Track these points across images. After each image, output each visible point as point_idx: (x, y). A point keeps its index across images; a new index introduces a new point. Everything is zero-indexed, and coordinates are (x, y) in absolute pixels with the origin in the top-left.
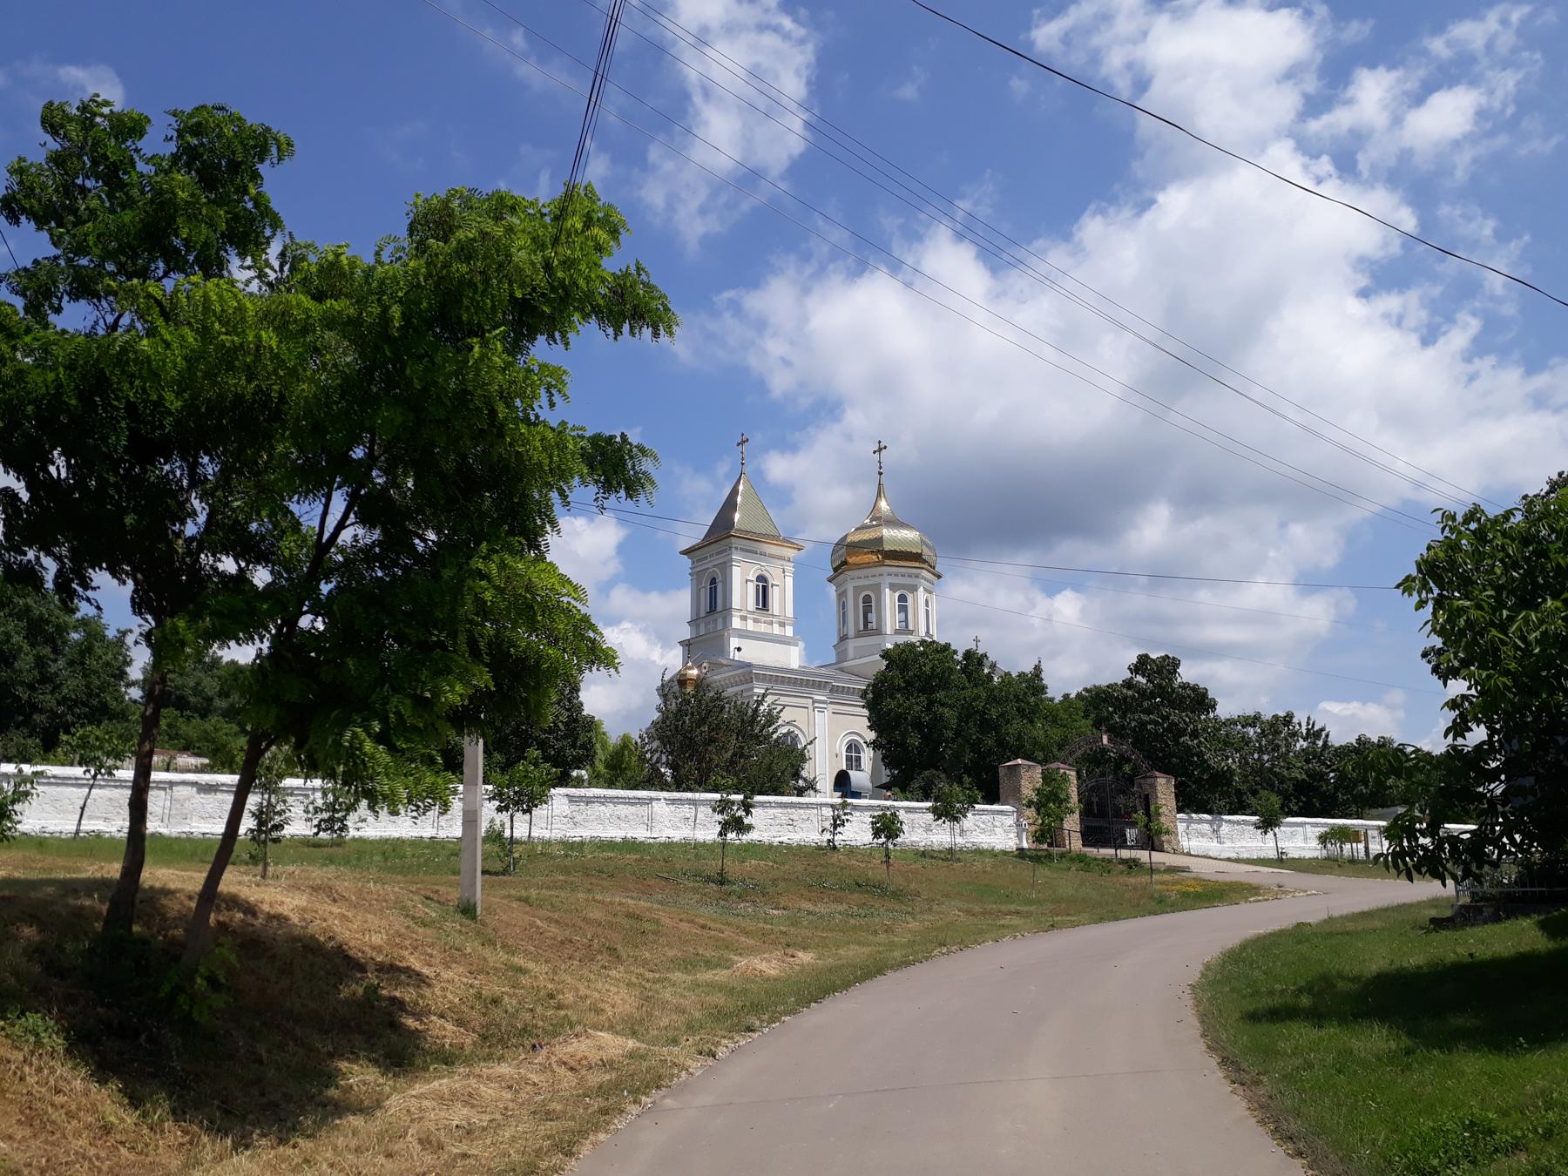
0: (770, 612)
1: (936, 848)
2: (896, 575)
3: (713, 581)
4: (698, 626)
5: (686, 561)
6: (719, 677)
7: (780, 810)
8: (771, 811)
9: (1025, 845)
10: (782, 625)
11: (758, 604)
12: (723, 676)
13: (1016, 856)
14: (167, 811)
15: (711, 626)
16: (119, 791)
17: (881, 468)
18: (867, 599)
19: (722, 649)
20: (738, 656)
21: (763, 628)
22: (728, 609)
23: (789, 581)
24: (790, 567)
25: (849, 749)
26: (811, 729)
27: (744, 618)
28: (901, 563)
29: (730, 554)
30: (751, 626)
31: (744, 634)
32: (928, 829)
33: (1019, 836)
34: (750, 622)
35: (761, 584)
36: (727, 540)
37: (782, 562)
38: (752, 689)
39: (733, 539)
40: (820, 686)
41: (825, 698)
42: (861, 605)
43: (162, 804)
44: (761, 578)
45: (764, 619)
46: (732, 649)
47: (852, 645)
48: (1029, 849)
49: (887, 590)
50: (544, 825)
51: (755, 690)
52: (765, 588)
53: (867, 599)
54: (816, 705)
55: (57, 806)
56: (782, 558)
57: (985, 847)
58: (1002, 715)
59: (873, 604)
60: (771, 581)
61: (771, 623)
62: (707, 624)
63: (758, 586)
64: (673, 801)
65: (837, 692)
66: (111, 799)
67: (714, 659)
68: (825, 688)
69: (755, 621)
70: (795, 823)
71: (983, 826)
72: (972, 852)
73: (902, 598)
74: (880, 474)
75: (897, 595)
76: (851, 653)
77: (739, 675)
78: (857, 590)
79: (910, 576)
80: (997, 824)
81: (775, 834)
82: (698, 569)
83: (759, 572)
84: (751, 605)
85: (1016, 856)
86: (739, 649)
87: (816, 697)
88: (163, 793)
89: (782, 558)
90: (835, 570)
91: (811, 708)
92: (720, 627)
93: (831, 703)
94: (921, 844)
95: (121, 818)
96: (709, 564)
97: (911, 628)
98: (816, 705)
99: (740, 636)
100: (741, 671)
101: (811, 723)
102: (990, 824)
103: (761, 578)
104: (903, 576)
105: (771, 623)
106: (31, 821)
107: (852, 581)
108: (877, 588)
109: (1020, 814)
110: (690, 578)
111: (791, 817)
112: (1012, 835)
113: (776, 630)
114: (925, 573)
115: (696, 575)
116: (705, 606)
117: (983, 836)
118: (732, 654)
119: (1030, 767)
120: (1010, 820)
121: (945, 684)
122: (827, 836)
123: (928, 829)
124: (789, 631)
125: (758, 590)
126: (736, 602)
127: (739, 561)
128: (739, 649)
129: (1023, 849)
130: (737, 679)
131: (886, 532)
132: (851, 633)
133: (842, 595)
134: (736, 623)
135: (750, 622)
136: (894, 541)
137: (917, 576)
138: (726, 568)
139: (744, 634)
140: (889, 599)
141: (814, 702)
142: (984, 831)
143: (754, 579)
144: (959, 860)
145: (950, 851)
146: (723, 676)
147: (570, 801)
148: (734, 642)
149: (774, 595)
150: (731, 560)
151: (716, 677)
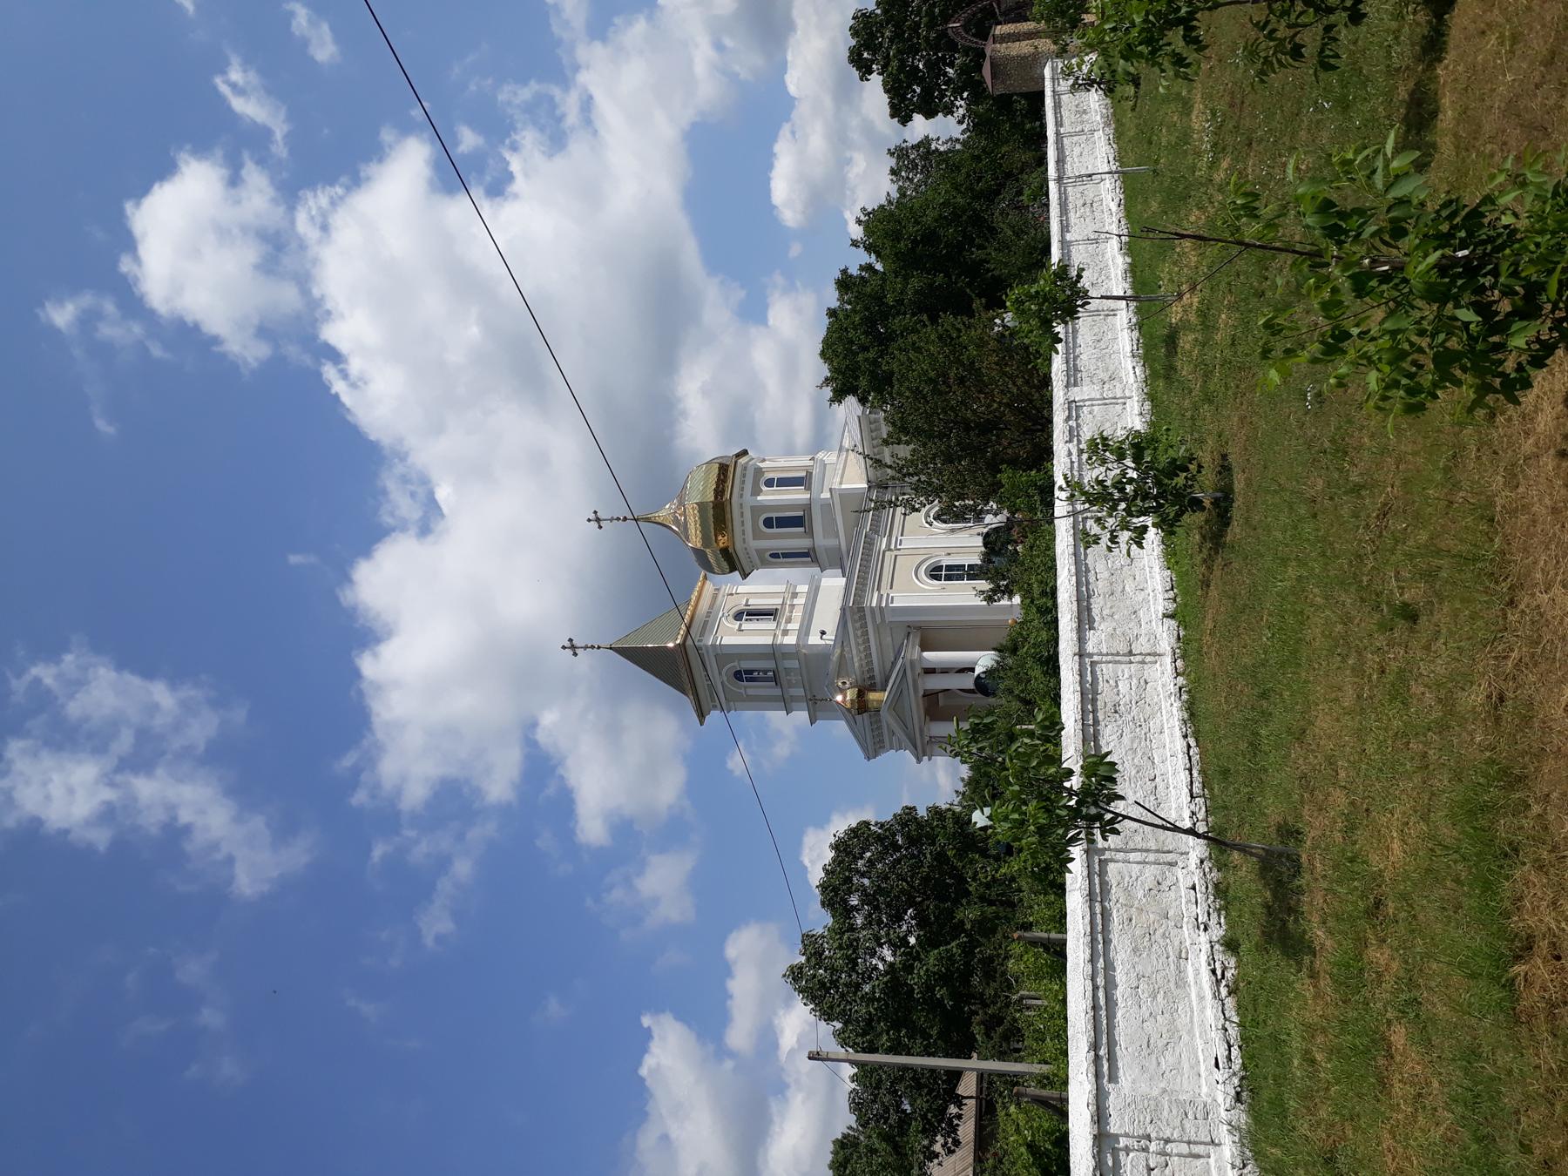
0: (779, 607)
2: (742, 489)
3: (738, 675)
5: (714, 716)
6: (856, 660)
10: (795, 595)
12: (854, 652)
14: (1152, 857)
15: (794, 678)
16: (1114, 937)
17: (618, 519)
18: (768, 523)
19: (822, 655)
20: (830, 637)
21: (798, 614)
22: (774, 652)
25: (938, 578)
26: (922, 551)
27: (785, 633)
29: (706, 646)
30: (794, 626)
31: (805, 630)
34: (789, 626)
35: (745, 617)
37: (720, 596)
41: (885, 540)
42: (775, 530)
43: (1136, 868)
44: (738, 616)
46: (823, 642)
47: (821, 541)
49: (759, 498)
50: (1119, 408)
51: (874, 604)
53: (768, 523)
54: (893, 547)
55: (1161, 1043)
56: (715, 597)
59: (774, 515)
60: (743, 607)
61: (792, 606)
66: (1135, 950)
67: (833, 666)
69: (789, 621)
70: (1089, 202)
73: (769, 483)
74: (599, 648)
75: (764, 488)
76: (831, 542)
77: (855, 629)
78: (757, 535)
83: (731, 618)
84: (769, 625)
86: (823, 633)
87: (883, 546)
88: (1111, 867)
89: (715, 597)
90: (733, 569)
92: (794, 664)
95: (1174, 932)
96: (720, 678)
97: (804, 474)
98: (893, 547)
99: (807, 634)
100: (850, 625)
101: (914, 552)
106: (1205, 1090)
107: (747, 539)
108: (757, 510)
113: (800, 601)
115: (728, 703)
118: (828, 642)
126: (768, 640)
128: (823, 633)
130: (862, 648)
132: (778, 692)
134: (791, 640)
135: (789, 626)
138: (726, 655)
139: (805, 630)
140: (769, 496)
141: (890, 550)
146: (854, 652)
147: (1076, 385)
148: (814, 639)
150: (713, 646)
151: (856, 665)
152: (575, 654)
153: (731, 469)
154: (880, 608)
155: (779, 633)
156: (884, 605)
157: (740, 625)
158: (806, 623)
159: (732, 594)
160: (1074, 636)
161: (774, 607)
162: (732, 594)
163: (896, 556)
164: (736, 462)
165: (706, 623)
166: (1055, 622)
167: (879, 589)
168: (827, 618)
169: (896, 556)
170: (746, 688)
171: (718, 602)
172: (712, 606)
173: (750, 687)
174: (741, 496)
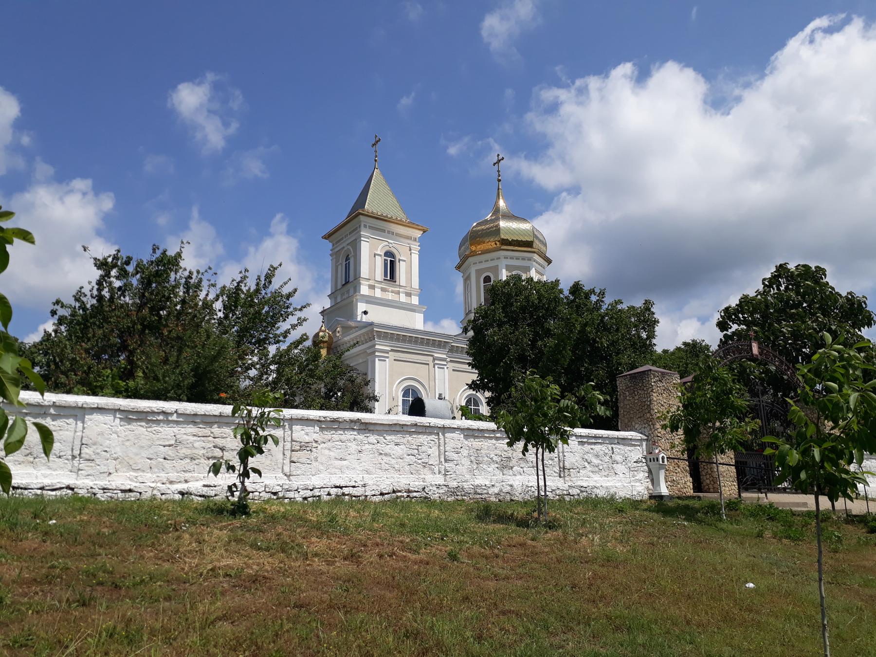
0: (397, 283)
1: (518, 498)
4: (336, 298)
5: (328, 245)
7: (191, 429)
8: (167, 432)
9: (664, 490)
10: (409, 295)
11: (386, 275)
13: (649, 509)
17: (499, 176)
19: (350, 313)
20: (365, 318)
21: (390, 296)
22: (357, 277)
23: (415, 258)
24: (416, 247)
26: (432, 383)
27: (372, 287)
28: (516, 248)
30: (378, 293)
31: (370, 300)
32: (505, 465)
33: (652, 477)
36: (356, 220)
38: (374, 345)
39: (361, 217)
40: (440, 345)
41: (445, 356)
42: (482, 284)
45: (391, 289)
48: (671, 497)
51: (377, 347)
52: (392, 263)
54: (436, 362)
57: (601, 493)
58: (613, 343)
60: (398, 257)
61: (398, 293)
62: (342, 295)
63: (385, 260)
64: (129, 416)
65: (457, 352)
68: (444, 347)
69: (383, 290)
71: (596, 461)
72: (579, 502)
74: (499, 181)
77: (363, 334)
78: (479, 272)
79: (523, 259)
80: (618, 458)
81: (173, 476)
82: (336, 250)
83: (387, 248)
84: (379, 274)
85: (649, 509)
86: (365, 313)
87: (436, 355)
91: (431, 365)
93: (451, 361)
94: (491, 491)
98: (436, 362)
99: (368, 302)
101: (432, 378)
102: (607, 459)
103: (389, 254)
104: (518, 259)
105: (398, 293)
109: (652, 442)
110: (331, 258)
111: (220, 442)
112: (642, 475)
113: (403, 298)
114: (536, 257)
115: (335, 255)
116: (341, 281)
117: (596, 477)
119: (663, 373)
120: (637, 453)
121: (551, 313)
122: (227, 479)
123: (505, 465)
124: (415, 300)
125: (386, 265)
127: (368, 237)
129: (661, 497)
131: (503, 224)
133: (467, 279)
134: (364, 290)
136: (509, 231)
137: (530, 259)
139: (370, 300)
141: (434, 360)
142: (597, 470)
143: (383, 254)
144: (551, 526)
145: (540, 502)
148: (361, 307)
149: (401, 270)
150: (360, 236)
151: (346, 339)
152: (494, 164)
153: (529, 249)
154: (374, 352)
155: (371, 282)
156: (377, 354)
157: (380, 255)
158: (373, 300)
159: (410, 250)
160: (129, 408)
161: (397, 280)
162: (410, 250)
163: (428, 364)
164: (534, 252)
165: (384, 231)
166: (149, 398)
167: (392, 350)
168: (378, 315)
169: (428, 364)
170: (341, 264)
171: (402, 239)
172: (398, 235)
173: (342, 267)
174: (506, 258)
